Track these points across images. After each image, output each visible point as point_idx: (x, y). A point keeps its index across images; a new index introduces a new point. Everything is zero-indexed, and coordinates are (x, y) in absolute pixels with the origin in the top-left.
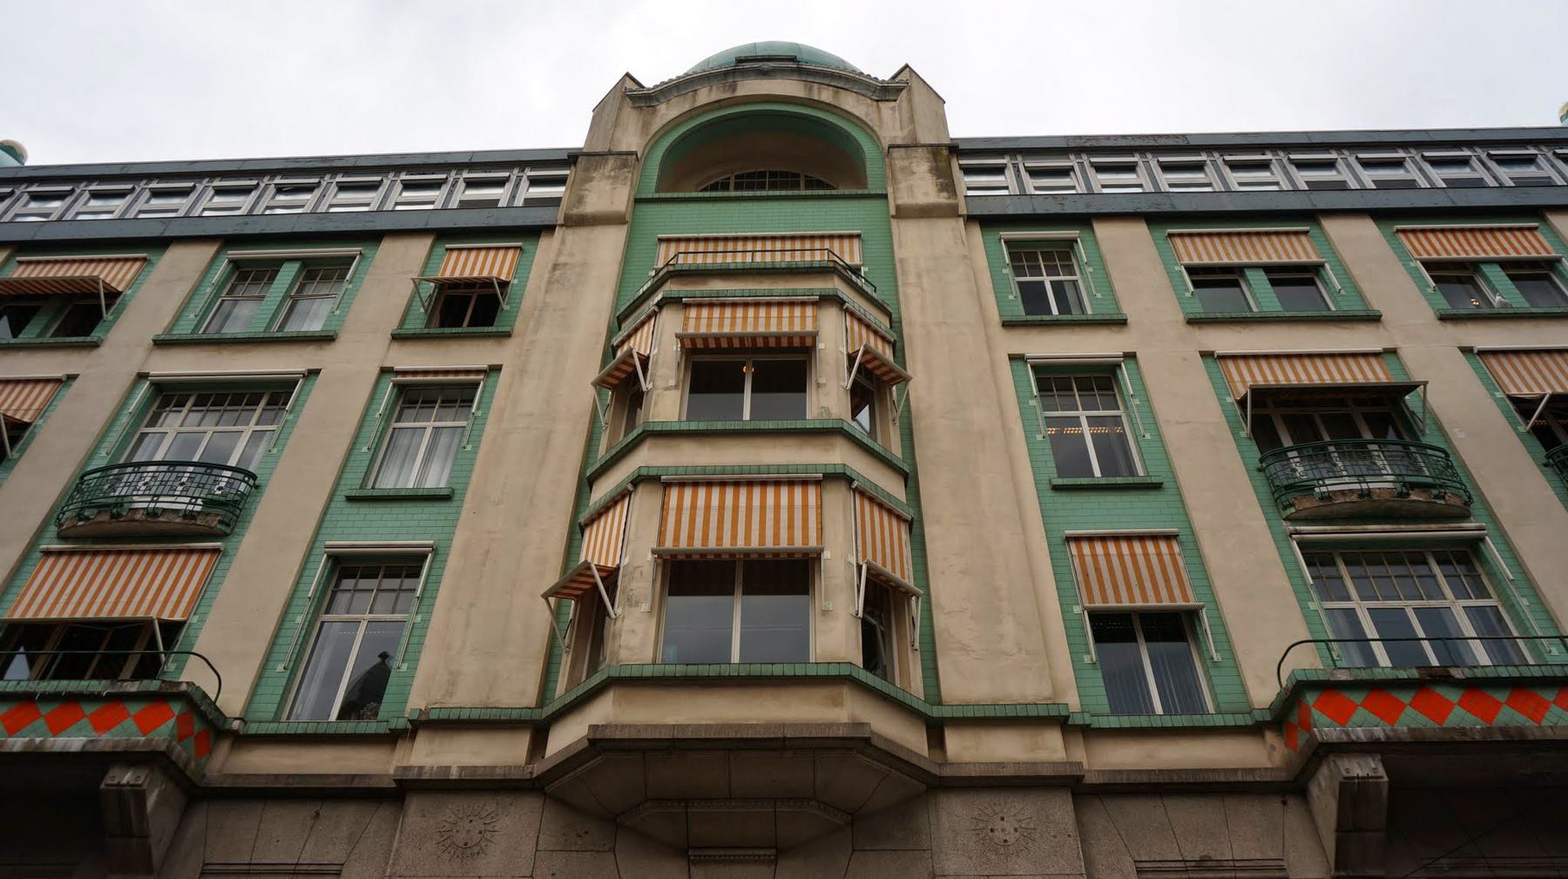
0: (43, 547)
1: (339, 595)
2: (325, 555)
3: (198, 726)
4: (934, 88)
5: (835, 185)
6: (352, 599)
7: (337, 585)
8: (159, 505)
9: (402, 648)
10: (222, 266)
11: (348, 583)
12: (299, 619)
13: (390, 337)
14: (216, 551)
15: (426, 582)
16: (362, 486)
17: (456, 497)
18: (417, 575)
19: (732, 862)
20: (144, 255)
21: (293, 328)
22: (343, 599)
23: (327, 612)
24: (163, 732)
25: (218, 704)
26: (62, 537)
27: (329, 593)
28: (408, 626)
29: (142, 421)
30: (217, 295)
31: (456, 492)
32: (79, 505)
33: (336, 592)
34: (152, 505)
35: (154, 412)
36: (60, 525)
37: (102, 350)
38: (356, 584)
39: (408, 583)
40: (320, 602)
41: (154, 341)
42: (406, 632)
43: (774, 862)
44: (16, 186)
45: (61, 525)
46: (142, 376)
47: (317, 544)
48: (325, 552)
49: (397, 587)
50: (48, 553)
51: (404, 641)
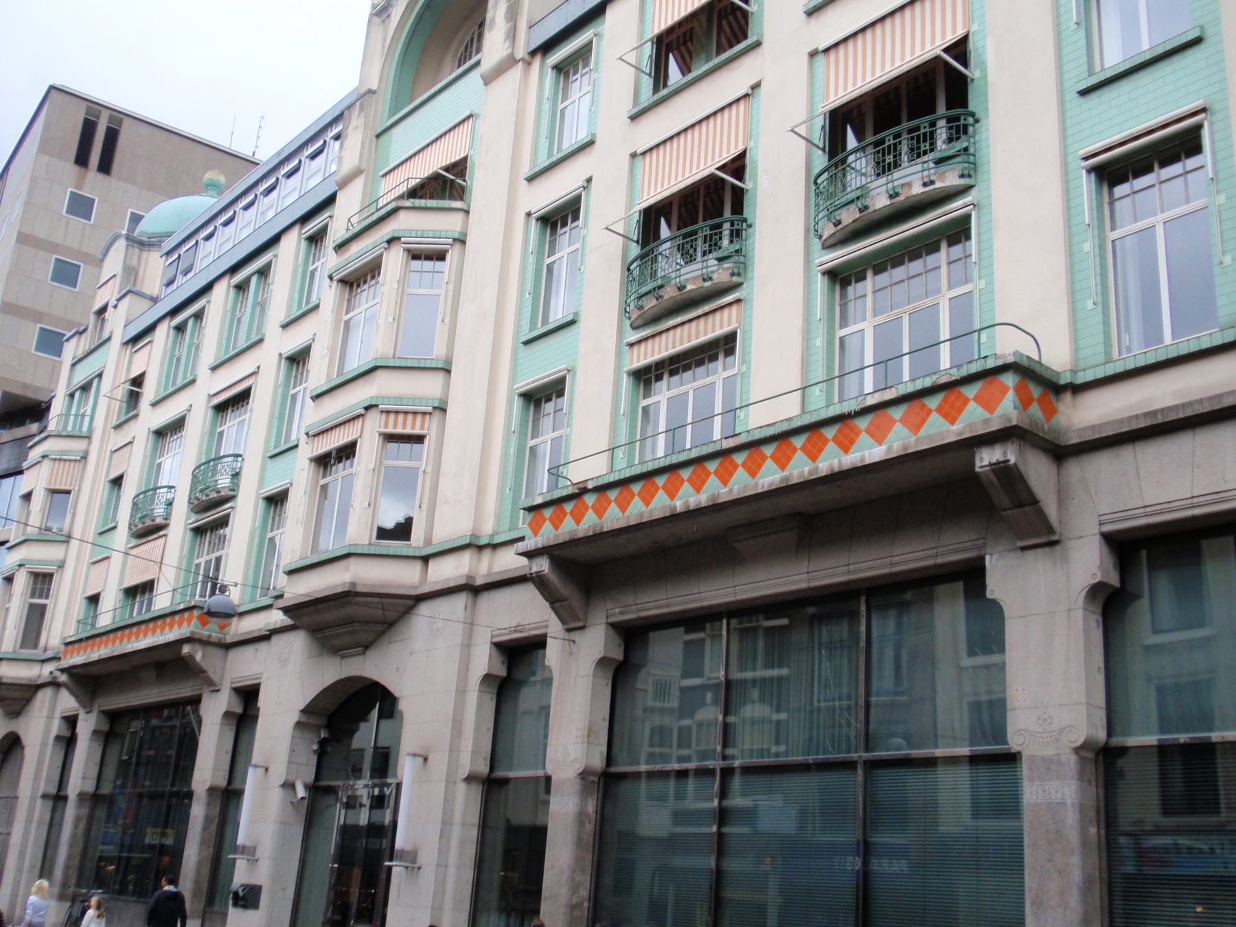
0: (817, 261)
1: (1117, 205)
2: (819, 274)
3: (1036, 391)
4: (310, 124)
5: (53, 395)
6: (1134, 203)
7: (1111, 194)
8: (896, 183)
9: (1216, 239)
10: (550, 75)
11: (1120, 190)
12: (1087, 247)
13: (805, 16)
14: (738, 301)
15: (1214, 154)
16: (1091, 73)
17: (1209, 33)
18: (968, 238)
19: (353, 656)
20: (328, 214)
21: (568, 144)
22: (1123, 207)
23: (1113, 228)
24: (1007, 409)
25: (1043, 362)
26: (635, 327)
27: (837, 309)
28: (976, 295)
29: (544, 254)
30: (555, 106)
31: (1205, 27)
32: (825, 212)
33: (846, 303)
34: (890, 185)
35: (550, 242)
36: (820, 237)
37: (198, 382)
38: (925, 266)
39: (1191, 163)
40: (1101, 220)
41: (629, 118)
42: (976, 303)
43: (364, 653)
44: (324, 135)
45: (820, 237)
46: (529, 214)
47: (1070, 158)
48: (1083, 168)
49: (1181, 171)
50: (631, 345)
51: (1215, 230)
